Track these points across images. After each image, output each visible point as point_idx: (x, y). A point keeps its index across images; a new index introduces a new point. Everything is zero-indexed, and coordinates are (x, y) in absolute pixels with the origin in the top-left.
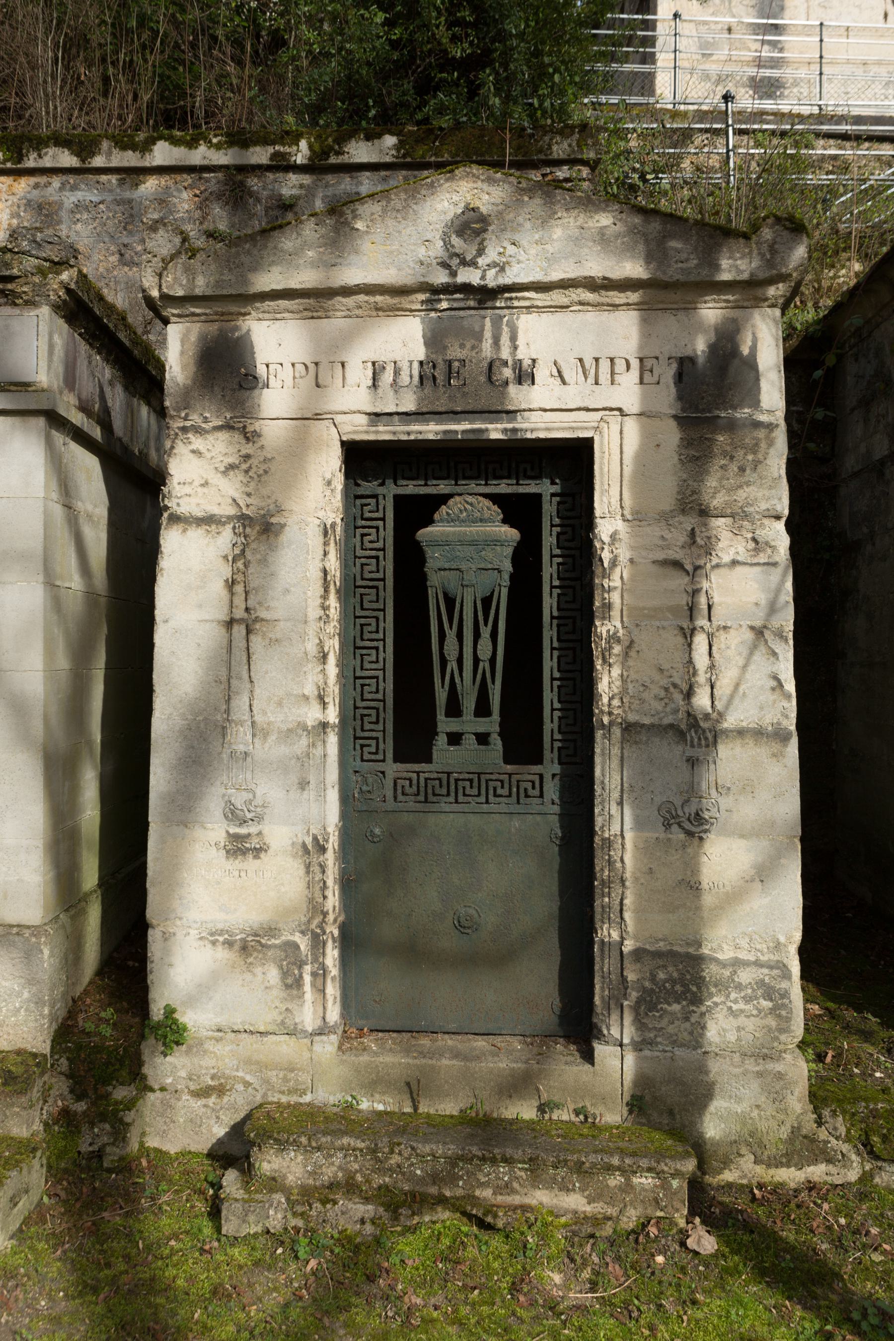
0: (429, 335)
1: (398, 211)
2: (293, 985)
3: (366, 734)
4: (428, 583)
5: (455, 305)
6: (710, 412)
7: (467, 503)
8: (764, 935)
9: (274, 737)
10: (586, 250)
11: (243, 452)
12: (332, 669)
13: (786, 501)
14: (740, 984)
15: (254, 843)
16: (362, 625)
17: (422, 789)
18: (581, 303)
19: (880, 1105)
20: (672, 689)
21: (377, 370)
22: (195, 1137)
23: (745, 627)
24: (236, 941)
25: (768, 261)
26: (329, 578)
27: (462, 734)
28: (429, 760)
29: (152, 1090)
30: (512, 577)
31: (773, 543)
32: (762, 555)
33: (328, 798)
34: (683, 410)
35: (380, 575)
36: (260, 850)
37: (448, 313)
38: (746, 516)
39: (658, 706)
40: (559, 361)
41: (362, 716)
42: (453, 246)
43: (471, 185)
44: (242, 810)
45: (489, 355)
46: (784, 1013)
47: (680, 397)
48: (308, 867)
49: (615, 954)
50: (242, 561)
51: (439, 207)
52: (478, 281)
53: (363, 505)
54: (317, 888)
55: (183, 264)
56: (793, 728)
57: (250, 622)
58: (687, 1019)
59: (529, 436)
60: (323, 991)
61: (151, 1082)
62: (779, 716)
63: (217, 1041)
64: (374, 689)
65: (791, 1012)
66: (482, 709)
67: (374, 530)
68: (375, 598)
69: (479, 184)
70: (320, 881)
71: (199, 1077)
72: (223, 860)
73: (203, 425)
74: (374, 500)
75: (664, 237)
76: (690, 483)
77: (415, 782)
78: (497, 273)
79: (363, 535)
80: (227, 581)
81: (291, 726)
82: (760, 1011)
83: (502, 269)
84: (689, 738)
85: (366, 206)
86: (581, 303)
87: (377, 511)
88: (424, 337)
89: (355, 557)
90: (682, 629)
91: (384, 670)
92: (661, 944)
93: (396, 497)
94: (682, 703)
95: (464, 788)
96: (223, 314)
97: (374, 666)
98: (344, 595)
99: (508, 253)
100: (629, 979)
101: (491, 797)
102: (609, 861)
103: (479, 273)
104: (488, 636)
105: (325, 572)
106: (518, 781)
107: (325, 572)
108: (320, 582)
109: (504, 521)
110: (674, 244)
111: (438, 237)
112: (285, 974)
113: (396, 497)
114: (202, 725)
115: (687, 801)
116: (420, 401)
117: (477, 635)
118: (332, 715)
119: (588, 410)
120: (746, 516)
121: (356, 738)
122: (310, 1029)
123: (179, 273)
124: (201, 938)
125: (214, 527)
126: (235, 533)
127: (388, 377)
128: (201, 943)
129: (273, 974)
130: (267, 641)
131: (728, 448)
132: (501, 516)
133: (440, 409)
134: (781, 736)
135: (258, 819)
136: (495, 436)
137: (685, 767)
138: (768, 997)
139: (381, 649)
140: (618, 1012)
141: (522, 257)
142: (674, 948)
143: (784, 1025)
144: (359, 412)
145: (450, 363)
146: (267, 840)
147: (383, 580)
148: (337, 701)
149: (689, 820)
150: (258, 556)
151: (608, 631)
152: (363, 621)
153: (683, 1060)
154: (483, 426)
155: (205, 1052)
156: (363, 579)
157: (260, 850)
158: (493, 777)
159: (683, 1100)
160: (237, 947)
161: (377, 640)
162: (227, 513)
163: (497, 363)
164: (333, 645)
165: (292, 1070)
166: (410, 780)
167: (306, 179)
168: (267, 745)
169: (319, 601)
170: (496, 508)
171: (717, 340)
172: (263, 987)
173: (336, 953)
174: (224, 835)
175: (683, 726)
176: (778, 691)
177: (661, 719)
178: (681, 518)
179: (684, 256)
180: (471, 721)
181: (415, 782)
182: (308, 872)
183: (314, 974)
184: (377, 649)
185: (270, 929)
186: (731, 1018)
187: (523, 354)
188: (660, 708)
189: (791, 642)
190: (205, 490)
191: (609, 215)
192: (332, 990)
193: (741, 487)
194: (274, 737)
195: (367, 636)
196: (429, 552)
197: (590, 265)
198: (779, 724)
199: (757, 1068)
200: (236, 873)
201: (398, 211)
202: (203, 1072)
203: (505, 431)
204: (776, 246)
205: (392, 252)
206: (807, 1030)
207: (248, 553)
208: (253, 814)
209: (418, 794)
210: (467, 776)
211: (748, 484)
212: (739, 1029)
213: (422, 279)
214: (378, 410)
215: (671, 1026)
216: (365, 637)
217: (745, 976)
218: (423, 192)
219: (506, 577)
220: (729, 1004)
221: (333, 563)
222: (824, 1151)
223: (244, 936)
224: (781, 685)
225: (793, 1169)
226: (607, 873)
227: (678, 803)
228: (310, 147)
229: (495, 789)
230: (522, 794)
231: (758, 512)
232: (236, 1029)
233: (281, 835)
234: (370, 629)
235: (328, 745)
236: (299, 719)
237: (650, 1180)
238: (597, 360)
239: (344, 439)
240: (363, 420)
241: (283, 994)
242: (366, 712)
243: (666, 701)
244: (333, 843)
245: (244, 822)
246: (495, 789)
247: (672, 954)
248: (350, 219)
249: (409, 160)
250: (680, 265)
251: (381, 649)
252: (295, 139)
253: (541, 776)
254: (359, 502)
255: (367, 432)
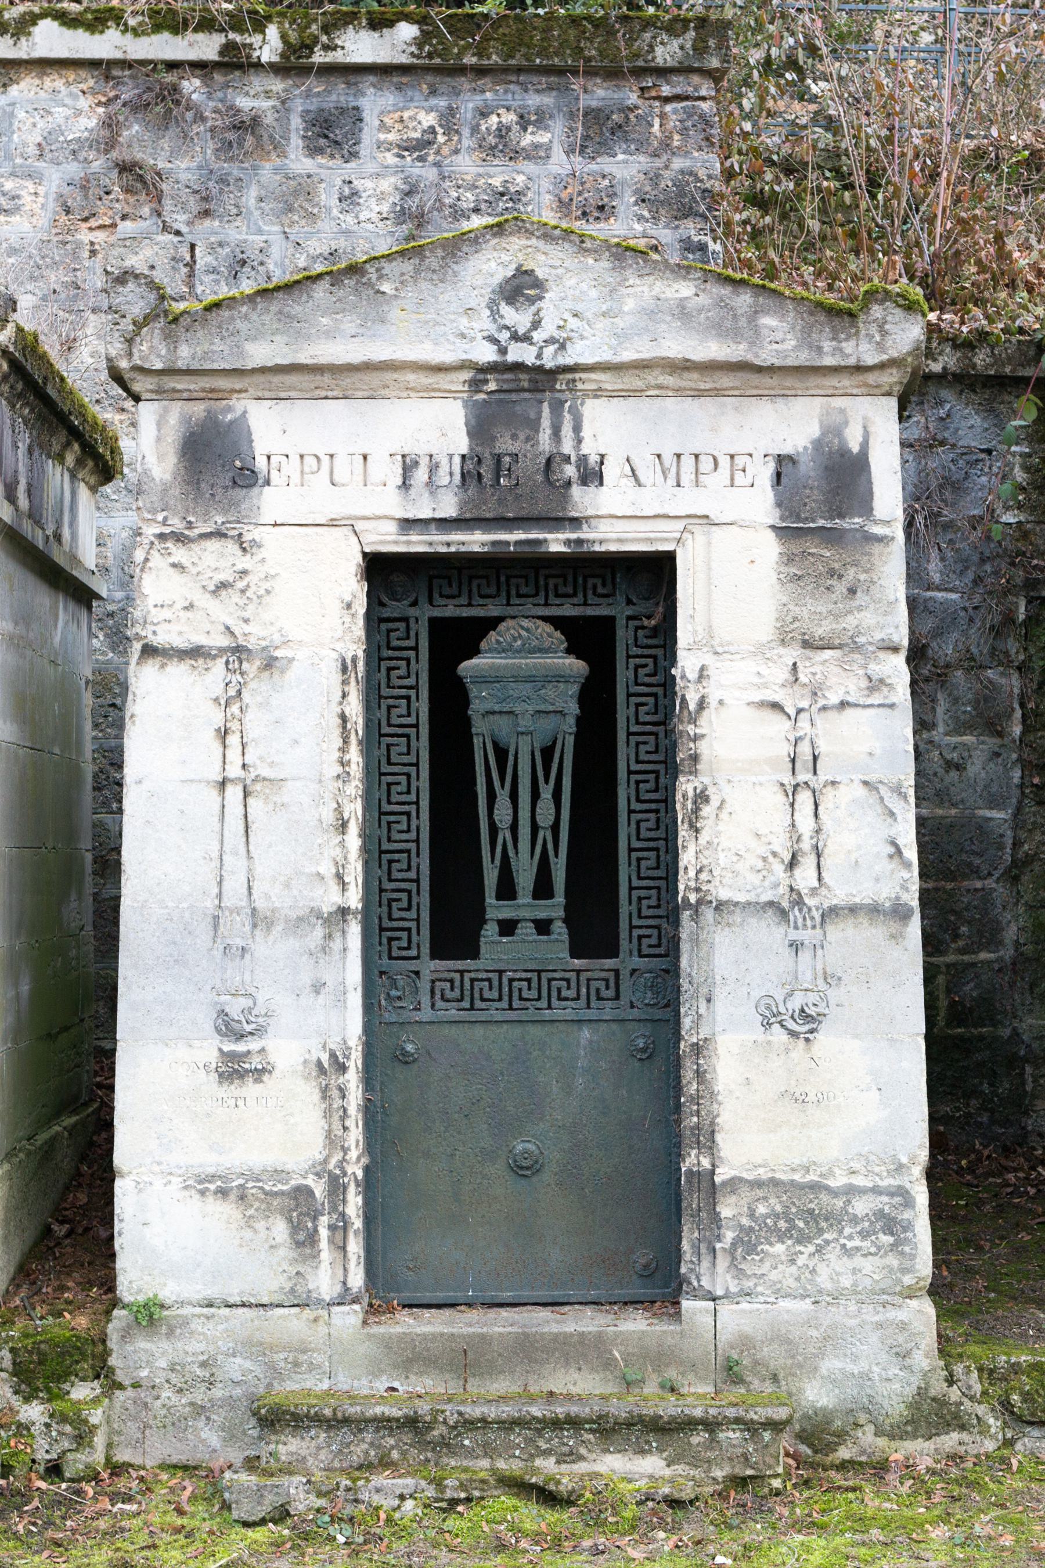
0: (473, 422)
1: (434, 271)
2: (305, 1242)
3: (395, 924)
4: (474, 730)
5: (505, 387)
6: (813, 521)
7: (522, 628)
8: (882, 1156)
9: (280, 928)
10: (664, 326)
11: (239, 567)
12: (354, 841)
13: (905, 631)
14: (855, 1216)
15: (256, 1062)
16: (389, 785)
17: (467, 993)
18: (660, 387)
19: (1023, 1358)
20: (771, 859)
21: (408, 467)
22: (179, 1445)
23: (857, 782)
24: (232, 1188)
25: (878, 343)
26: (349, 726)
27: (517, 921)
28: (475, 955)
29: (121, 1387)
30: (579, 720)
31: (888, 681)
32: (876, 694)
33: (349, 1004)
34: (782, 518)
35: (411, 720)
36: (264, 1070)
37: (497, 396)
38: (857, 648)
39: (755, 879)
40: (633, 457)
41: (390, 901)
42: (502, 317)
43: (524, 242)
44: (239, 1022)
45: (547, 448)
46: (907, 1249)
47: (779, 504)
48: (325, 1091)
49: (704, 1185)
50: (238, 705)
51: (485, 267)
52: (533, 361)
53: (389, 631)
54: (336, 1117)
55: (161, 329)
56: (915, 903)
57: (248, 782)
58: (793, 1261)
59: (597, 548)
60: (344, 1248)
61: (120, 1376)
62: (898, 889)
63: (208, 1318)
64: (405, 867)
65: (916, 1248)
66: (543, 889)
67: (404, 663)
68: (405, 750)
69: (534, 241)
70: (339, 1109)
71: (183, 1366)
72: (215, 1085)
73: (187, 532)
74: (404, 624)
75: (756, 312)
76: (791, 607)
77: (457, 983)
78: (556, 352)
79: (389, 669)
80: (218, 730)
81: (301, 913)
82: (879, 1249)
83: (563, 347)
84: (792, 918)
85: (394, 263)
86: (660, 387)
87: (408, 638)
88: (466, 425)
89: (380, 697)
90: (782, 785)
91: (417, 841)
92: (761, 1171)
93: (433, 621)
94: (782, 875)
95: (520, 990)
96: (212, 391)
97: (404, 836)
98: (367, 746)
99: (569, 327)
100: (722, 1216)
101: (554, 1000)
102: (697, 1071)
103: (534, 350)
104: (550, 796)
105: (343, 718)
106: (588, 980)
107: (343, 718)
108: (338, 731)
109: (569, 651)
110: (768, 321)
111: (483, 305)
112: (295, 1228)
113: (433, 621)
114: (187, 915)
115: (790, 994)
116: (463, 505)
117: (535, 795)
118: (354, 899)
119: (666, 516)
120: (857, 648)
121: (382, 929)
122: (327, 1298)
123: (156, 341)
124: (186, 1188)
125: (201, 661)
126: (228, 669)
127: (421, 475)
128: (187, 1193)
129: (280, 1229)
130: (271, 806)
131: (836, 566)
132: (566, 644)
133: (488, 515)
134: (900, 913)
135: (258, 1032)
136: (556, 548)
137: (787, 953)
138: (889, 1230)
139: (414, 814)
140: (709, 1258)
141: (588, 332)
142: (777, 1175)
143: (908, 1264)
144: (386, 517)
145: (498, 459)
146: (272, 1058)
147: (416, 726)
148: (360, 881)
149: (792, 1017)
150: (259, 699)
151: (695, 788)
152: (390, 779)
153: (788, 1311)
154: (541, 536)
155: (192, 1333)
156: (389, 725)
157: (264, 1070)
158: (556, 975)
159: (790, 1362)
160: (233, 1196)
161: (409, 803)
162: (218, 644)
163: (558, 459)
164: (354, 810)
165: (304, 1351)
166: (452, 981)
167: (278, 85)
168: (271, 937)
169: (338, 755)
170: (558, 634)
171: (823, 434)
172: (267, 1246)
173: (360, 1200)
174: (216, 1053)
175: (785, 904)
176: (896, 859)
177: (758, 896)
178: (782, 650)
179: (779, 336)
180: (529, 905)
181: (457, 983)
182: (324, 1098)
183: (332, 1228)
184: (408, 814)
185: (276, 1171)
186: (845, 1259)
187: (590, 448)
188: (757, 882)
189: (912, 800)
190: (189, 614)
191: (690, 284)
192: (355, 1247)
193: (850, 612)
194: (280, 928)
195: (395, 798)
196: (473, 691)
197: (668, 344)
198: (898, 898)
199: (876, 1318)
200: (232, 1102)
201: (434, 271)
202: (189, 1359)
203: (568, 542)
204: (887, 327)
205: (427, 322)
206: (936, 1265)
207: (245, 694)
208: (253, 1026)
209: (461, 1000)
210: (524, 975)
211: (860, 609)
212: (855, 1271)
213: (464, 357)
214: (410, 515)
215: (774, 1272)
216: (393, 800)
217: (861, 1207)
218: (465, 249)
219: (571, 721)
220: (842, 1241)
221: (355, 708)
222: (956, 1416)
223: (241, 1181)
224: (899, 852)
225: (920, 1440)
226: (695, 1087)
227: (779, 997)
228: (284, 37)
229: (559, 990)
230: (593, 997)
231: (871, 643)
232: (231, 1301)
233: (288, 1049)
234: (399, 789)
235: (349, 937)
236: (312, 904)
237: (738, 1434)
238: (679, 456)
239: (367, 550)
240: (392, 527)
241: (292, 1254)
242: (395, 895)
243: (764, 873)
244: (355, 1061)
245: (241, 1036)
246: (559, 990)
247: (774, 1182)
248: (374, 280)
249: (437, 61)
250: (775, 346)
251: (414, 814)
252: (259, 25)
253: (617, 972)
254: (384, 626)
255: (396, 542)
